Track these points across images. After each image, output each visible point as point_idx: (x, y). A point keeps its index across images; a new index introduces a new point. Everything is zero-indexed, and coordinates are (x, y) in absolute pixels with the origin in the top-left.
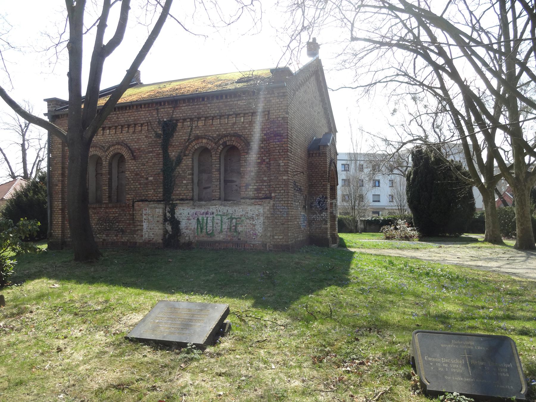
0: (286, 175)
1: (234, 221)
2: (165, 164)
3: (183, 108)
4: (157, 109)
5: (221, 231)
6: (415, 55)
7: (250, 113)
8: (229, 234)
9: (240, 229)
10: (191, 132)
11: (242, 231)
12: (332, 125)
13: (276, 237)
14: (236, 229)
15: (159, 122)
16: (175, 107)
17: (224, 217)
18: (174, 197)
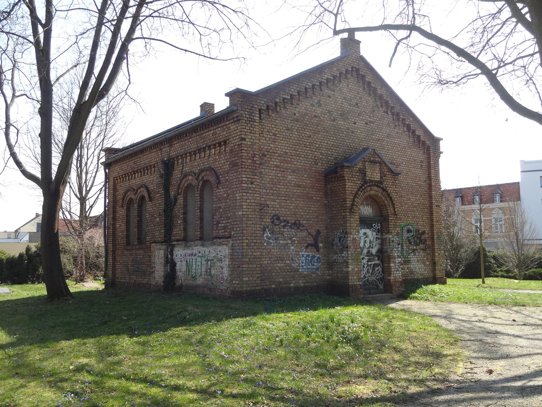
0: (241, 210)
1: (209, 262)
2: (166, 204)
3: (176, 145)
4: (161, 149)
5: (201, 275)
6: (409, 32)
7: (216, 143)
8: (206, 277)
9: (213, 272)
10: (183, 169)
11: (214, 275)
12: (419, 132)
13: (234, 282)
14: (210, 272)
15: (162, 162)
16: (171, 146)
17: (203, 259)
18: (173, 238)
